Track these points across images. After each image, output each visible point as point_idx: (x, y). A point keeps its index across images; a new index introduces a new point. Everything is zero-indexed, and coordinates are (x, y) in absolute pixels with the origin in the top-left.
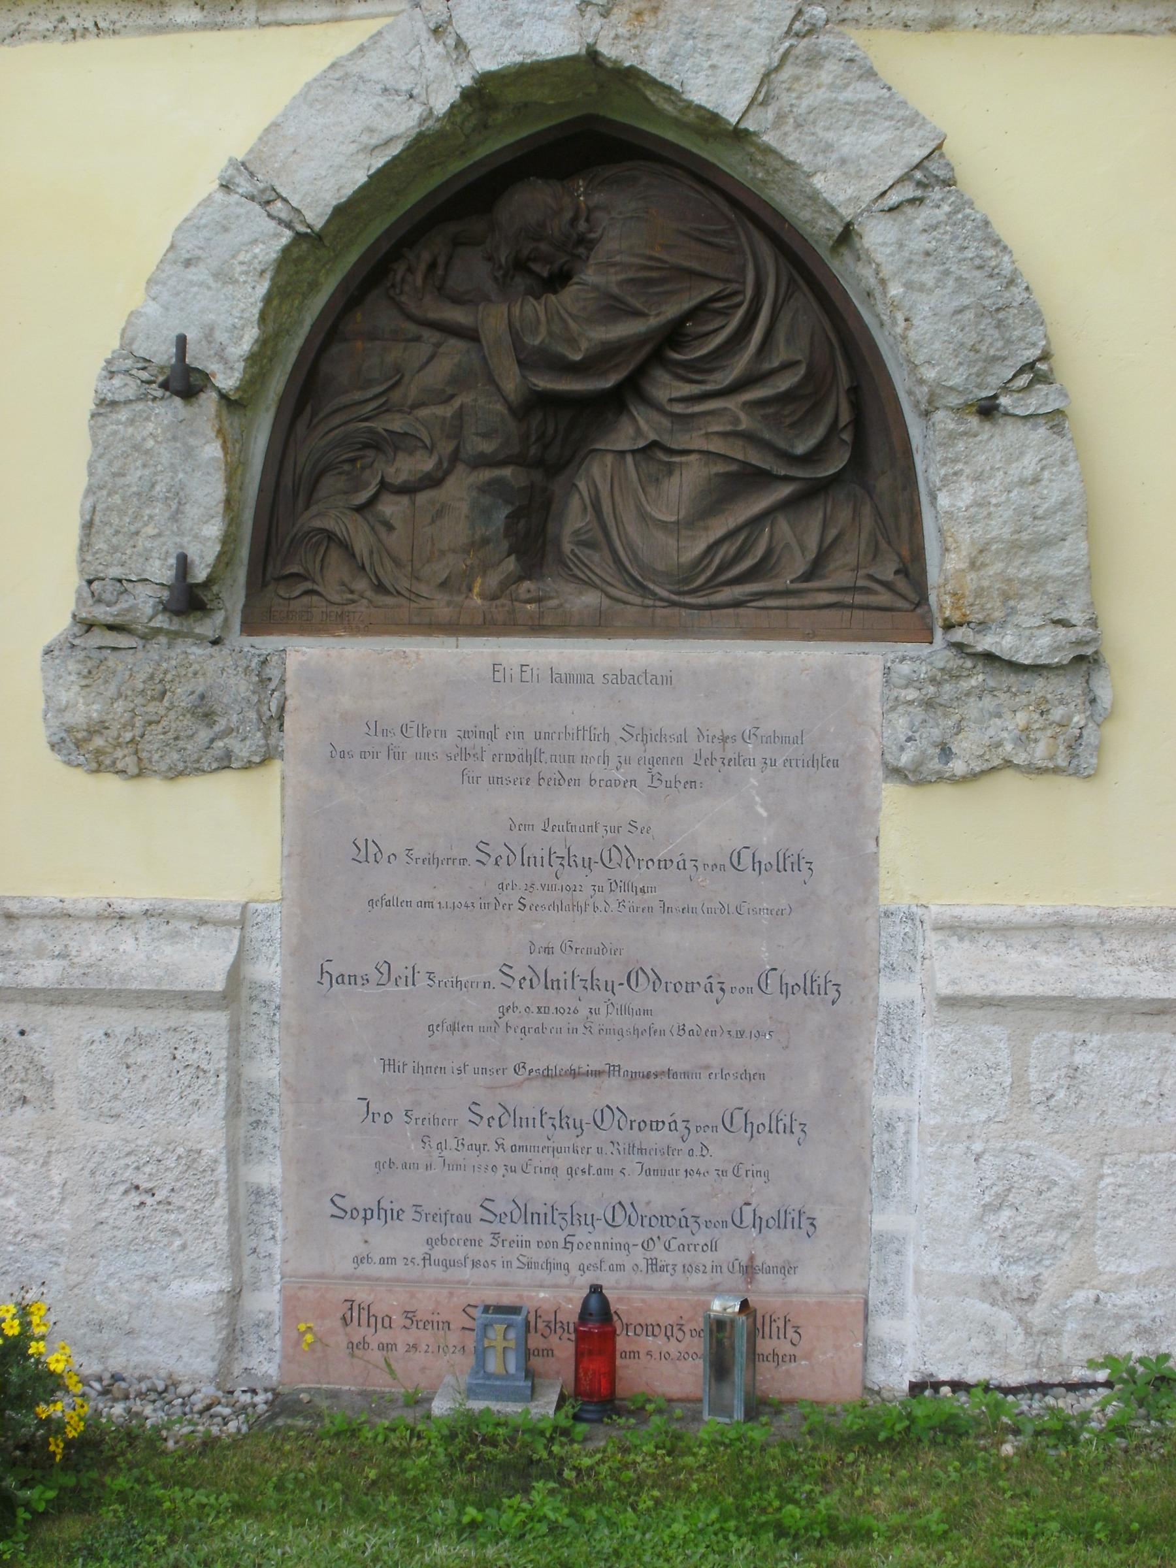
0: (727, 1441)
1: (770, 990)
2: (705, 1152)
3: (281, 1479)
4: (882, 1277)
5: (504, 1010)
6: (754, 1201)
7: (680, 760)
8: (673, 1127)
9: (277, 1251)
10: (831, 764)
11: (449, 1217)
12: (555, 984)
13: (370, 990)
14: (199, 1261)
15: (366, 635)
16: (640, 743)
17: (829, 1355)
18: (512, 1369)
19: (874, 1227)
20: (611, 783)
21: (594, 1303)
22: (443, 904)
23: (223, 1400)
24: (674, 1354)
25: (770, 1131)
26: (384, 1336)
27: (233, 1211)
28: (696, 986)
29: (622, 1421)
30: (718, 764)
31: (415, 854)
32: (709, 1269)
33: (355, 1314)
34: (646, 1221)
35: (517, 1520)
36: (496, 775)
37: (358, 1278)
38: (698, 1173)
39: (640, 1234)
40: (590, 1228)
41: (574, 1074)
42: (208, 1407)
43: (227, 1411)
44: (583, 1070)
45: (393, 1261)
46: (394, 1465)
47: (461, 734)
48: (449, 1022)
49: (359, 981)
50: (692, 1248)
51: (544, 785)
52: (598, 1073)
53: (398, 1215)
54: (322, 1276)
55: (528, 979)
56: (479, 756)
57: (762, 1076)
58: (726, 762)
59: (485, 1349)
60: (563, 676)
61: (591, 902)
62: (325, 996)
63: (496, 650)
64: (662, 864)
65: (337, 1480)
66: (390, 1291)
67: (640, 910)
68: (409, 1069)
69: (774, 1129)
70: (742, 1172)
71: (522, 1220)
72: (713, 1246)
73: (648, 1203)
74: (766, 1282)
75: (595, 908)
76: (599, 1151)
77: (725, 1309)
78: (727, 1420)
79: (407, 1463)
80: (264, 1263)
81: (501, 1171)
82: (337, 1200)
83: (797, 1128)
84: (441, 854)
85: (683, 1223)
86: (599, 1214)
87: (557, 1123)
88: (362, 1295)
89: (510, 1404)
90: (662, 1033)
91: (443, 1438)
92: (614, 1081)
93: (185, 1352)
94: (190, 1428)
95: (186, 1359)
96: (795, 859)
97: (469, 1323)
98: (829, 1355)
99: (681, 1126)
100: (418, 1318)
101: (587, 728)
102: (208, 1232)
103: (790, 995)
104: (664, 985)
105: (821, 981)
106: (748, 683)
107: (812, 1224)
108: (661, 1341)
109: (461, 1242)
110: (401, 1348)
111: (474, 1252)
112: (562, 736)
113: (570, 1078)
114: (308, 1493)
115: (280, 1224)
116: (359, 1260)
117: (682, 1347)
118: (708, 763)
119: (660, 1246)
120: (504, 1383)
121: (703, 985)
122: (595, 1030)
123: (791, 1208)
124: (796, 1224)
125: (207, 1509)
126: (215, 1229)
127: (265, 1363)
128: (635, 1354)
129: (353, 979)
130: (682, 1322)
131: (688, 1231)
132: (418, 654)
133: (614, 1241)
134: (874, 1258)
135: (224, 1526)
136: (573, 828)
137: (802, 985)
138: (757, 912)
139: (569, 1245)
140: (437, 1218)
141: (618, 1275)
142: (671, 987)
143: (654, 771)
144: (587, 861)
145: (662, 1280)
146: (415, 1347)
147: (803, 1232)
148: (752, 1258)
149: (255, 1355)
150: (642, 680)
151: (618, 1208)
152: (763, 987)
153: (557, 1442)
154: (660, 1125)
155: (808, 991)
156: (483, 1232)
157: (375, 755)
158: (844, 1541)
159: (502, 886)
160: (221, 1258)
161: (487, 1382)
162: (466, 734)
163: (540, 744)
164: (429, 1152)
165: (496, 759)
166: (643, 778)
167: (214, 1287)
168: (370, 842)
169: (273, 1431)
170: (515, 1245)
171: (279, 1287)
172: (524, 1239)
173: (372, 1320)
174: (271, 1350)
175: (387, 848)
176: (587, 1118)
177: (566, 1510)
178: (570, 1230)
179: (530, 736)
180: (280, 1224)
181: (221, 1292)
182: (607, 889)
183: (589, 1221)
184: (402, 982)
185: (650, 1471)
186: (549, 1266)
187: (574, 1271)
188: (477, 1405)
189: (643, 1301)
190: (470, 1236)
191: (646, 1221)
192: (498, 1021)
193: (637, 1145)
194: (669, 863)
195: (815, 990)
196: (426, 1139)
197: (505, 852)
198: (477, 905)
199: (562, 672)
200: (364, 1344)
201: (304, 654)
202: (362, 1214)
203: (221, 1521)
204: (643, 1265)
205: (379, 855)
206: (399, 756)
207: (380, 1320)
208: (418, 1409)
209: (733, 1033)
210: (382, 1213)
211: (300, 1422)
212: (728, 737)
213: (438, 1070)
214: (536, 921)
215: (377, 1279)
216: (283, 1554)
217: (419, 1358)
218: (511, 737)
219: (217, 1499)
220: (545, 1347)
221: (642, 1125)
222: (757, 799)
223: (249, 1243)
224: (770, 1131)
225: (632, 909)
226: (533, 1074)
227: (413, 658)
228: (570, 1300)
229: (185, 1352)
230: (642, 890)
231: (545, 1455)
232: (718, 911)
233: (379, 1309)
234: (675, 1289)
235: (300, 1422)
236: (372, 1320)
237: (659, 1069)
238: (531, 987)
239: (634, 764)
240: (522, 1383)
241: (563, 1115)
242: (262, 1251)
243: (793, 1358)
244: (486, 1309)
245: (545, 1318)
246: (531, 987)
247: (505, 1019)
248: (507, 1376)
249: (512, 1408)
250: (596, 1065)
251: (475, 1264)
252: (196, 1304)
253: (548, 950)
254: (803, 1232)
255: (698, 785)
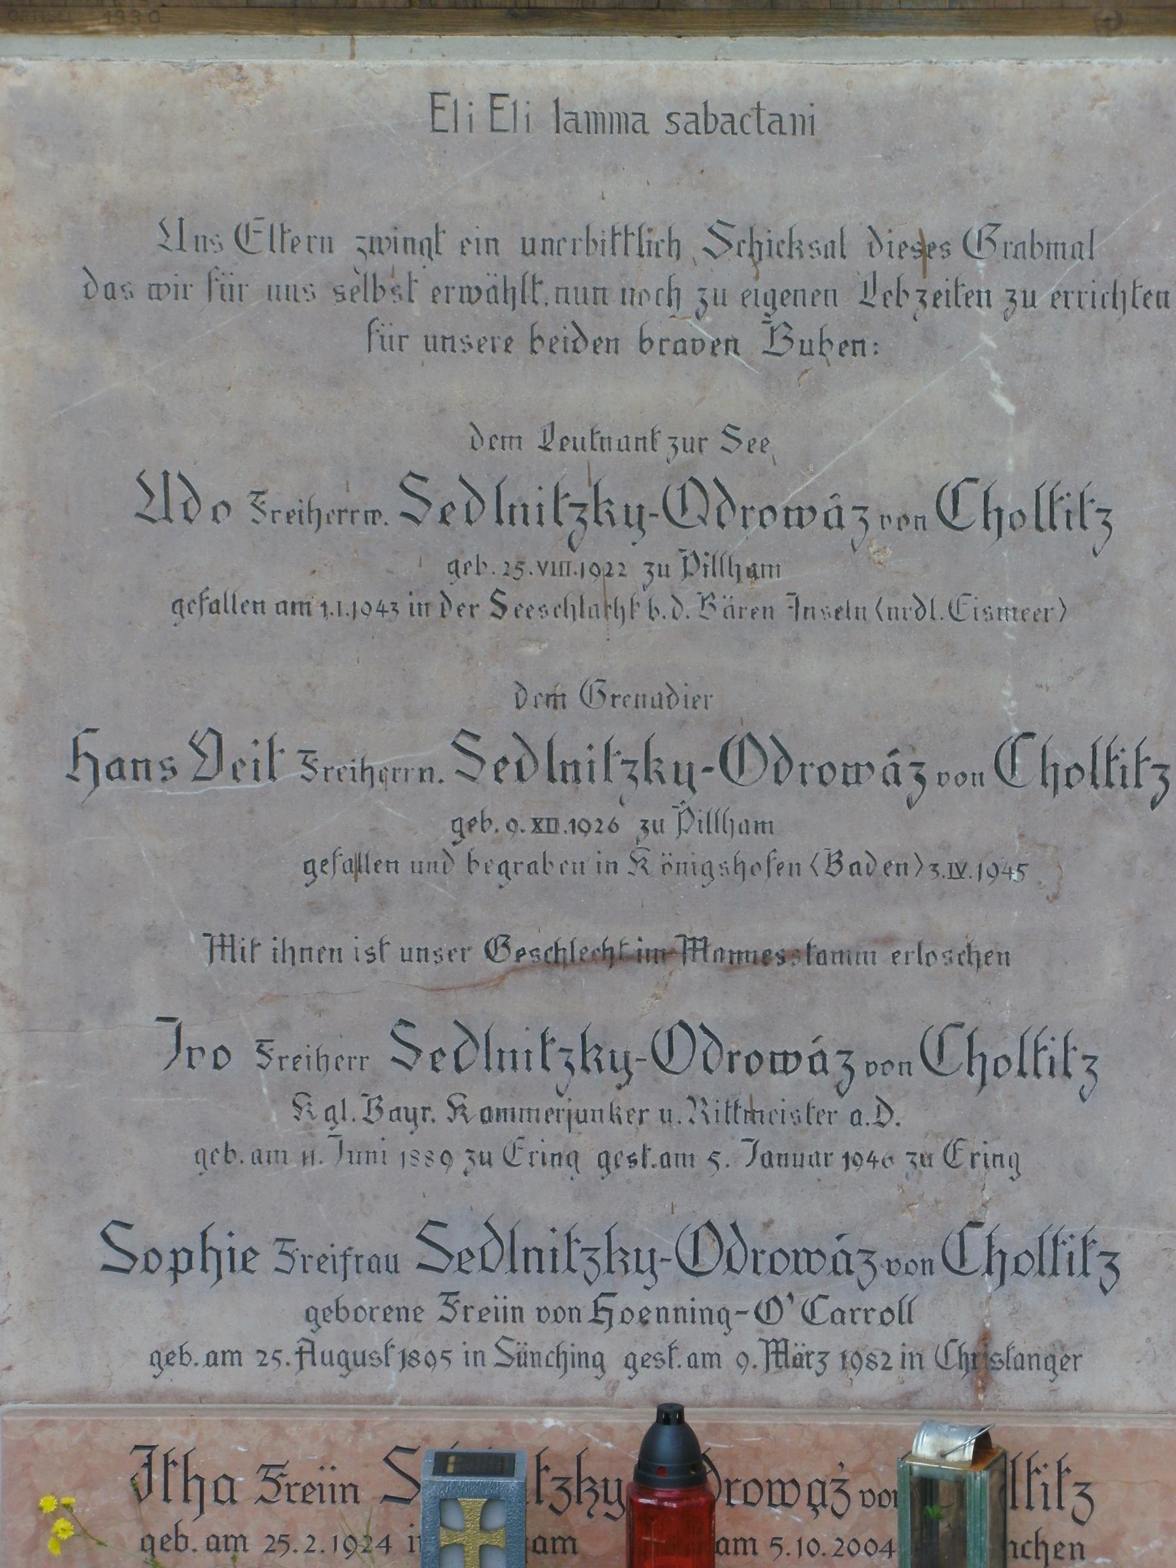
1: (1019, 779)
2: (885, 1117)
5: (463, 827)
6: (990, 1219)
7: (830, 296)
8: (818, 1065)
10: (1152, 301)
11: (351, 1262)
12: (570, 770)
13: (183, 790)
15: (155, 31)
16: (746, 260)
17: (1155, 1544)
20: (684, 347)
21: (667, 1440)
22: (332, 607)
25: (1022, 1073)
26: (219, 1521)
28: (864, 770)
30: (911, 304)
31: (270, 501)
32: (895, 1361)
33: (158, 1477)
34: (764, 1263)
36: (440, 332)
37: (161, 1398)
38: (872, 1160)
40: (648, 1279)
41: (610, 957)
44: (631, 949)
45: (233, 1357)
47: (365, 244)
48: (348, 853)
49: (156, 771)
50: (859, 1316)
51: (542, 350)
52: (660, 956)
53: (244, 1262)
54: (85, 1396)
55: (513, 760)
56: (404, 291)
57: (1004, 958)
58: (929, 299)
59: (441, 1550)
60: (582, 118)
61: (642, 598)
62: (82, 805)
63: (438, 62)
64: (794, 517)
66: (230, 1423)
67: (747, 614)
68: (264, 954)
69: (1029, 1067)
70: (963, 1158)
71: (506, 1264)
72: (903, 1314)
73: (768, 1224)
75: (653, 612)
76: (665, 1116)
77: (943, 1455)
81: (461, 1162)
82: (115, 1233)
83: (1077, 1066)
84: (325, 502)
85: (841, 1266)
86: (666, 1249)
87: (577, 1062)
90: (795, 869)
92: (695, 971)
96: (1073, 503)
97: (403, 1488)
98: (1155, 1544)
99: (834, 1063)
101: (633, 229)
103: (1063, 789)
104: (797, 769)
105: (1129, 759)
106: (975, 130)
107: (1110, 1266)
108: (799, 1515)
109: (378, 1315)
111: (405, 1335)
112: (581, 246)
113: (603, 967)
116: (162, 1359)
117: (844, 1528)
118: (891, 300)
119: (793, 1314)
121: (879, 770)
122: (654, 865)
123: (1066, 1232)
128: (746, 1545)
129: (142, 769)
131: (852, 1280)
132: (268, 72)
133: (698, 1305)
136: (604, 444)
137: (1088, 768)
138: (992, 614)
139: (603, 1316)
140: (327, 1265)
141: (703, 1376)
142: (812, 774)
143: (776, 320)
144: (634, 512)
146: (285, 1540)
147: (1092, 1282)
148: (985, 1337)
150: (750, 124)
151: (705, 1237)
152: (1006, 772)
154: (792, 1061)
155: (1101, 780)
157: (182, 291)
159: (455, 568)
162: (375, 245)
163: (536, 265)
164: (308, 1127)
165: (441, 298)
166: (752, 335)
168: (174, 480)
170: (490, 1317)
172: (510, 1303)
173: (194, 1486)
175: (211, 489)
176: (639, 1050)
178: (606, 1283)
179: (510, 247)
182: (677, 570)
183: (645, 1264)
184: (246, 772)
186: (563, 1359)
187: (615, 1370)
189: (762, 1432)
190: (396, 1302)
191: (764, 1263)
192: (451, 849)
193: (744, 1104)
194: (807, 516)
195: (1116, 778)
196: (302, 1101)
197: (461, 495)
198: (404, 609)
199: (580, 109)
200: (177, 1540)
201: (20, 72)
202: (168, 1261)
204: (758, 1353)
205: (193, 505)
206: (232, 293)
207: (209, 1487)
209: (943, 869)
212: (933, 246)
213: (326, 956)
214: (530, 640)
215: (202, 1398)
218: (471, 249)
220: (557, 1532)
221: (754, 1061)
222: (995, 376)
224: (1022, 1073)
225: (730, 612)
226: (526, 959)
227: (259, 80)
228: (608, 1433)
230: (752, 573)
232: (911, 615)
233: (207, 1464)
234: (824, 1404)
236: (194, 1486)
237: (788, 945)
238: (520, 777)
239: (734, 307)
241: (589, 1045)
244: (441, 1463)
245: (556, 1471)
246: (520, 777)
247: (466, 845)
250: (655, 940)
251: (408, 1359)
253: (554, 700)
254: (1092, 1282)
255: (869, 349)
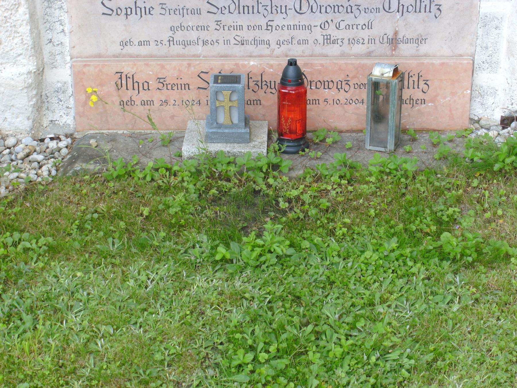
0: (388, 170)
3: (83, 222)
4: (485, 45)
9: (66, 40)
11: (185, 11)
14: (11, 53)
18: (236, 120)
19: (481, 11)
23: (38, 149)
24: (343, 101)
26: (144, 96)
27: (32, 15)
29: (312, 154)
32: (366, 41)
33: (124, 82)
35: (255, 254)
37: (124, 56)
39: (319, 19)
40: (284, 15)
42: (28, 155)
43: (40, 157)
45: (147, 43)
46: (160, 202)
50: (355, 27)
53: (149, 11)
54: (99, 56)
65: (121, 219)
72: (369, 26)
74: (405, 49)
77: (383, 75)
78: (383, 149)
79: (169, 199)
80: (58, 49)
85: (349, 10)
86: (290, 6)
88: (128, 69)
89: (236, 145)
91: (192, 174)
93: (8, 115)
94: (16, 174)
95: (9, 120)
98: (448, 98)
100: (167, 82)
102: (16, 32)
107: (439, 9)
109: (195, 28)
110: (157, 104)
111: (204, 35)
114: (101, 234)
115: (67, 21)
116: (124, 44)
117: (348, 96)
119: (332, 26)
120: (231, 131)
124: (428, 9)
125: (30, 253)
126: (21, 30)
127: (65, 116)
128: (316, 101)
130: (348, 79)
131: (352, 15)
133: (301, 24)
134: (480, 32)
135: (43, 269)
139: (269, 28)
140: (177, 12)
145: (334, 50)
146: (166, 102)
148: (396, 33)
149: (57, 111)
153: (271, 175)
156: (210, 20)
158: (490, 265)
160: (27, 50)
161: (219, 131)
167: (25, 70)
169: (73, 174)
170: (232, 29)
171: (69, 65)
172: (238, 24)
173: (136, 85)
174: (68, 107)
177: (288, 242)
178: (270, 17)
180: (67, 21)
181: (29, 73)
183: (283, 10)
185: (340, 199)
186: (256, 42)
187: (273, 45)
188: (214, 147)
189: (322, 65)
202: (124, 11)
203: (41, 265)
204: (321, 39)
207: (141, 85)
208: (171, 148)
210: (138, 10)
211: (92, 167)
215: (137, 56)
216: (89, 294)
217: (170, 109)
219: (37, 243)
220: (255, 98)
223: (46, 36)
228: (271, 66)
229: (8, 115)
231: (264, 187)
233: (140, 78)
234: (343, 55)
235: (92, 167)
236: (136, 85)
240: (243, 131)
242: (56, 41)
243: (424, 101)
248: (233, 125)
249: (236, 148)
251: (205, 43)
252: (13, 82)
254: (432, 14)
